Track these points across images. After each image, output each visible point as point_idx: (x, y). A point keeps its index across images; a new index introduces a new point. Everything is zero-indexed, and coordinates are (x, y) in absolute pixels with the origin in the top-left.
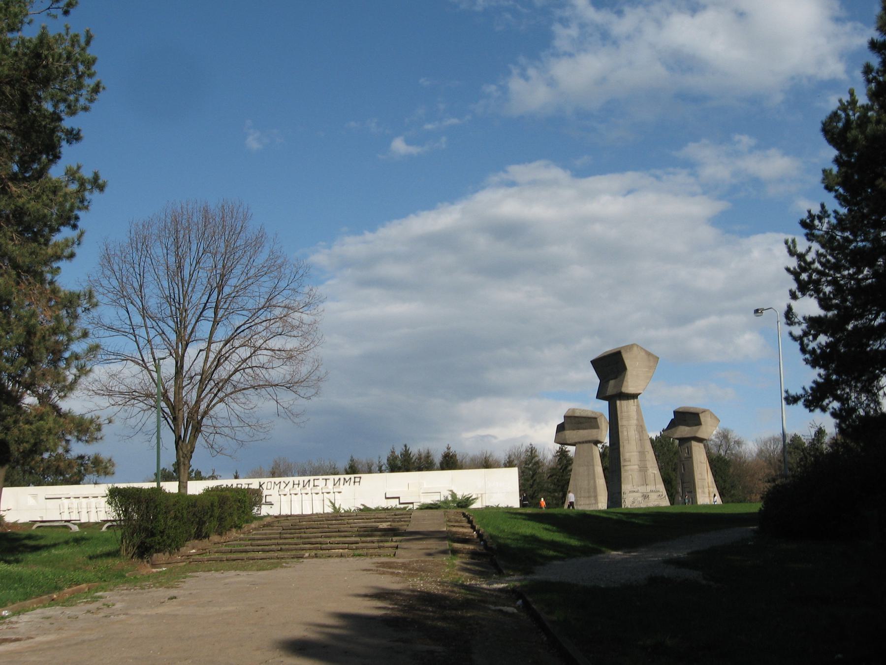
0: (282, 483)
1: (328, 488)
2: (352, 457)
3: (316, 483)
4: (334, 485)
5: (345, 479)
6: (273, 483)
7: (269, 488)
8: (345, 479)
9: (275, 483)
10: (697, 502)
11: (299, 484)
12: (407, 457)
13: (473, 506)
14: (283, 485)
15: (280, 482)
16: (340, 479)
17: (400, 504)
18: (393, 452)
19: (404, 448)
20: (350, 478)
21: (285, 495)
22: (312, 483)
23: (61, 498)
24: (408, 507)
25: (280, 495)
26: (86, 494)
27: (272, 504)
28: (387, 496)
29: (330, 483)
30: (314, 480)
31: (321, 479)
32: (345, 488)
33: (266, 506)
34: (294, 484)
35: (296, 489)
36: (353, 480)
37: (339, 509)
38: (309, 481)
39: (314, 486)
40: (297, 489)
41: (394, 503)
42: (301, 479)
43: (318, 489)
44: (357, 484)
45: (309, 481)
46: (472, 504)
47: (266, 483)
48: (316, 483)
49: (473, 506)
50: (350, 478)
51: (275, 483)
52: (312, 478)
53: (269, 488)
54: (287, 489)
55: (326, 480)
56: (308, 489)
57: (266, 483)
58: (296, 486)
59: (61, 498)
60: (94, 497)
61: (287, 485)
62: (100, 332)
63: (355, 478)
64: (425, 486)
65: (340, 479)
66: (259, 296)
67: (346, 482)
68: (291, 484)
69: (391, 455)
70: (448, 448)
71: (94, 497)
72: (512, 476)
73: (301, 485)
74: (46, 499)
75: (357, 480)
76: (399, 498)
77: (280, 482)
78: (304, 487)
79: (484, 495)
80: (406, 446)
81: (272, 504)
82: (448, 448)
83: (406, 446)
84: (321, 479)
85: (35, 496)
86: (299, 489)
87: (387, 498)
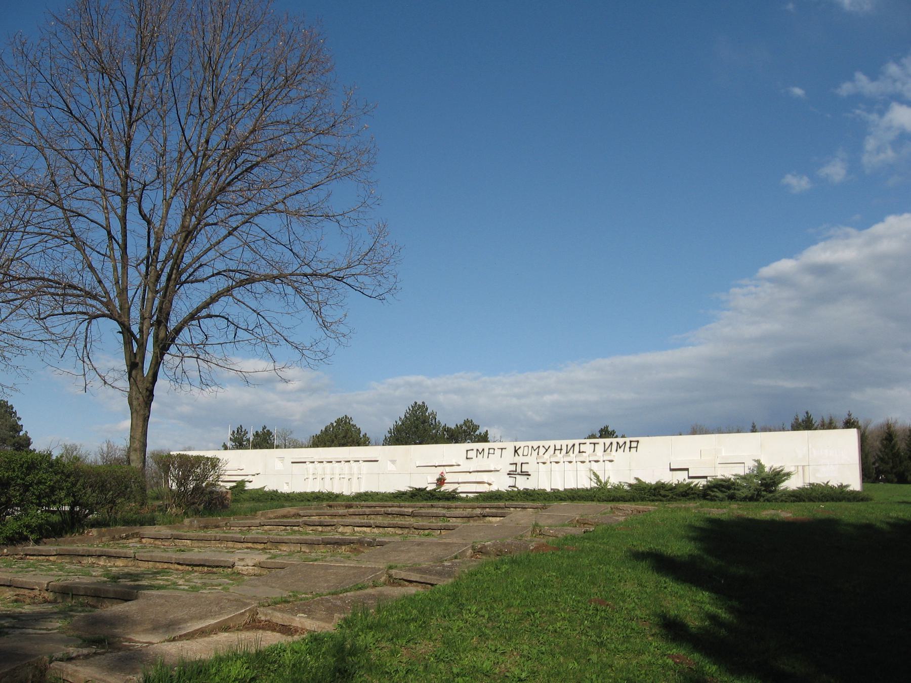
0: (541, 448)
1: (596, 455)
2: (754, 424)
3: (583, 448)
4: (605, 451)
5: (618, 443)
6: (530, 448)
7: (525, 453)
8: (618, 443)
9: (532, 447)
10: (858, 492)
11: (561, 449)
12: (808, 424)
13: (783, 486)
14: (542, 450)
15: (539, 447)
16: (611, 443)
17: (690, 478)
18: (797, 419)
19: (806, 415)
20: (625, 443)
21: (544, 463)
22: (577, 447)
23: (305, 462)
24: (692, 483)
25: (538, 463)
26: (357, 457)
27: (529, 475)
28: (515, 465)
29: (600, 448)
30: (580, 444)
31: (588, 443)
32: (618, 456)
33: (522, 477)
34: (555, 450)
35: (557, 456)
36: (628, 445)
37: (606, 483)
38: (574, 445)
39: (580, 452)
40: (559, 456)
41: (723, 477)
42: (564, 443)
43: (583, 457)
44: (633, 450)
45: (574, 445)
46: (784, 481)
47: (522, 448)
48: (583, 448)
49: (783, 486)
50: (625, 443)
51: (532, 447)
52: (577, 442)
53: (525, 453)
54: (547, 456)
55: (594, 444)
56: (572, 456)
57: (522, 448)
58: (558, 452)
59: (305, 462)
60: (355, 461)
61: (547, 450)
62: (23, 286)
63: (631, 442)
64: (723, 454)
65: (611, 443)
66: (25, 232)
67: (620, 448)
68: (551, 450)
69: (795, 422)
70: (850, 415)
71: (355, 461)
72: (850, 439)
73: (564, 451)
74: (292, 463)
75: (634, 444)
76: (687, 470)
77: (539, 447)
78: (567, 453)
79: (806, 468)
80: (807, 413)
81: (529, 475)
82: (850, 415)
83: (807, 413)
84: (588, 443)
85: (282, 459)
86: (574, 455)
87: (672, 470)
